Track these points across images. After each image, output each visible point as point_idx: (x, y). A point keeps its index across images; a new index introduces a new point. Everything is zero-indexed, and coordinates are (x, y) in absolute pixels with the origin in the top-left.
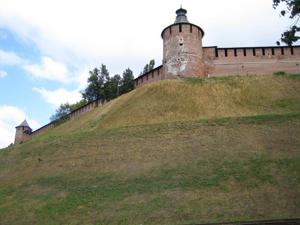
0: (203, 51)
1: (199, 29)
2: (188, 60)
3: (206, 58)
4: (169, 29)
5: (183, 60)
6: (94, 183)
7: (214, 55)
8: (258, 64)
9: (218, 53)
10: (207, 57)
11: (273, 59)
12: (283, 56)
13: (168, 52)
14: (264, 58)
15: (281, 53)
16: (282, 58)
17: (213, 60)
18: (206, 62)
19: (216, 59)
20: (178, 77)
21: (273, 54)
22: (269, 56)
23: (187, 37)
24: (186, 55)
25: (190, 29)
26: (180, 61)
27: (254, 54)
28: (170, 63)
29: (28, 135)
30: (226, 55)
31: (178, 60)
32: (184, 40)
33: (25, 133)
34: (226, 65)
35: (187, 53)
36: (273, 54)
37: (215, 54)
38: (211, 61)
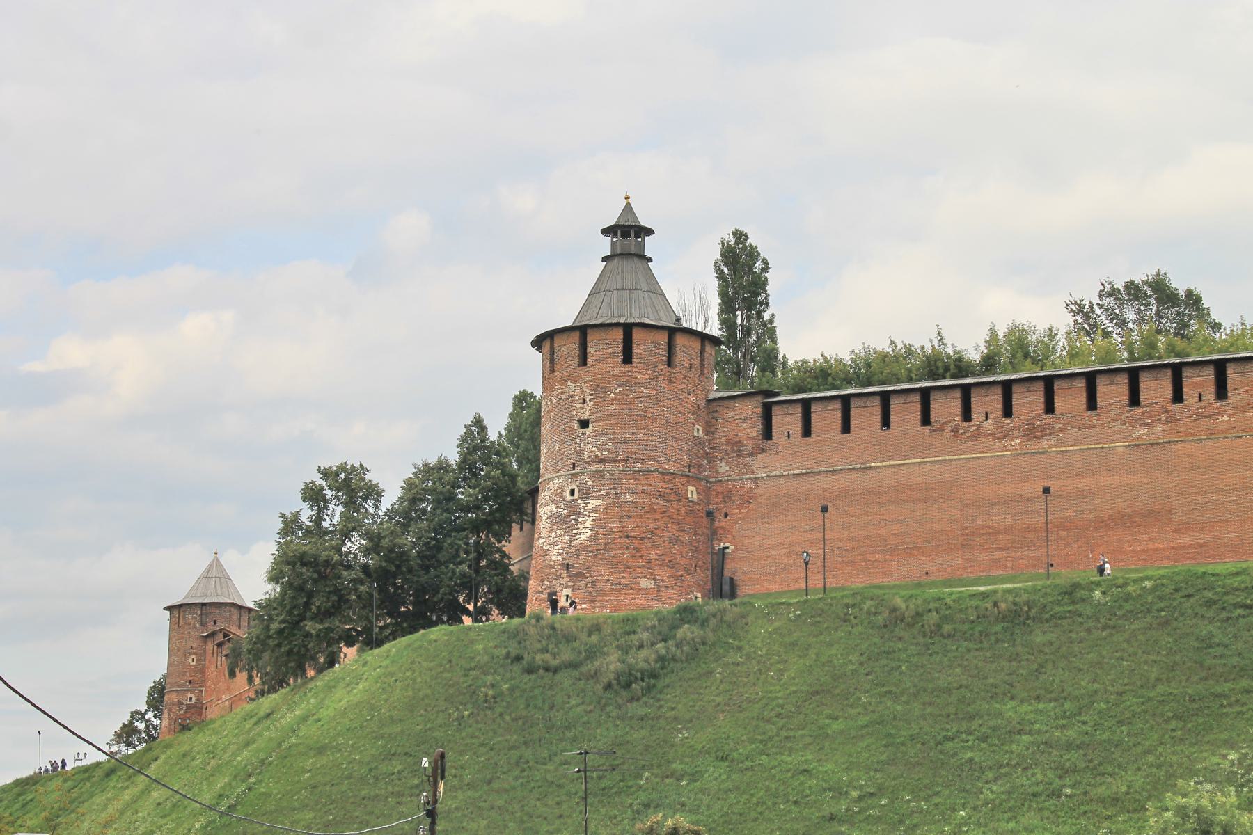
2: (608, 494)
5: (586, 496)
6: (1046, 654)
7: (756, 431)
10: (728, 442)
12: (1048, 419)
14: (964, 437)
16: (1046, 432)
17: (751, 454)
18: (723, 464)
19: (763, 450)
20: (564, 573)
22: (989, 425)
23: (605, 389)
24: (602, 471)
31: (568, 497)
32: (596, 404)
34: (801, 479)
35: (602, 460)
36: (1008, 412)
37: (760, 427)
38: (741, 460)
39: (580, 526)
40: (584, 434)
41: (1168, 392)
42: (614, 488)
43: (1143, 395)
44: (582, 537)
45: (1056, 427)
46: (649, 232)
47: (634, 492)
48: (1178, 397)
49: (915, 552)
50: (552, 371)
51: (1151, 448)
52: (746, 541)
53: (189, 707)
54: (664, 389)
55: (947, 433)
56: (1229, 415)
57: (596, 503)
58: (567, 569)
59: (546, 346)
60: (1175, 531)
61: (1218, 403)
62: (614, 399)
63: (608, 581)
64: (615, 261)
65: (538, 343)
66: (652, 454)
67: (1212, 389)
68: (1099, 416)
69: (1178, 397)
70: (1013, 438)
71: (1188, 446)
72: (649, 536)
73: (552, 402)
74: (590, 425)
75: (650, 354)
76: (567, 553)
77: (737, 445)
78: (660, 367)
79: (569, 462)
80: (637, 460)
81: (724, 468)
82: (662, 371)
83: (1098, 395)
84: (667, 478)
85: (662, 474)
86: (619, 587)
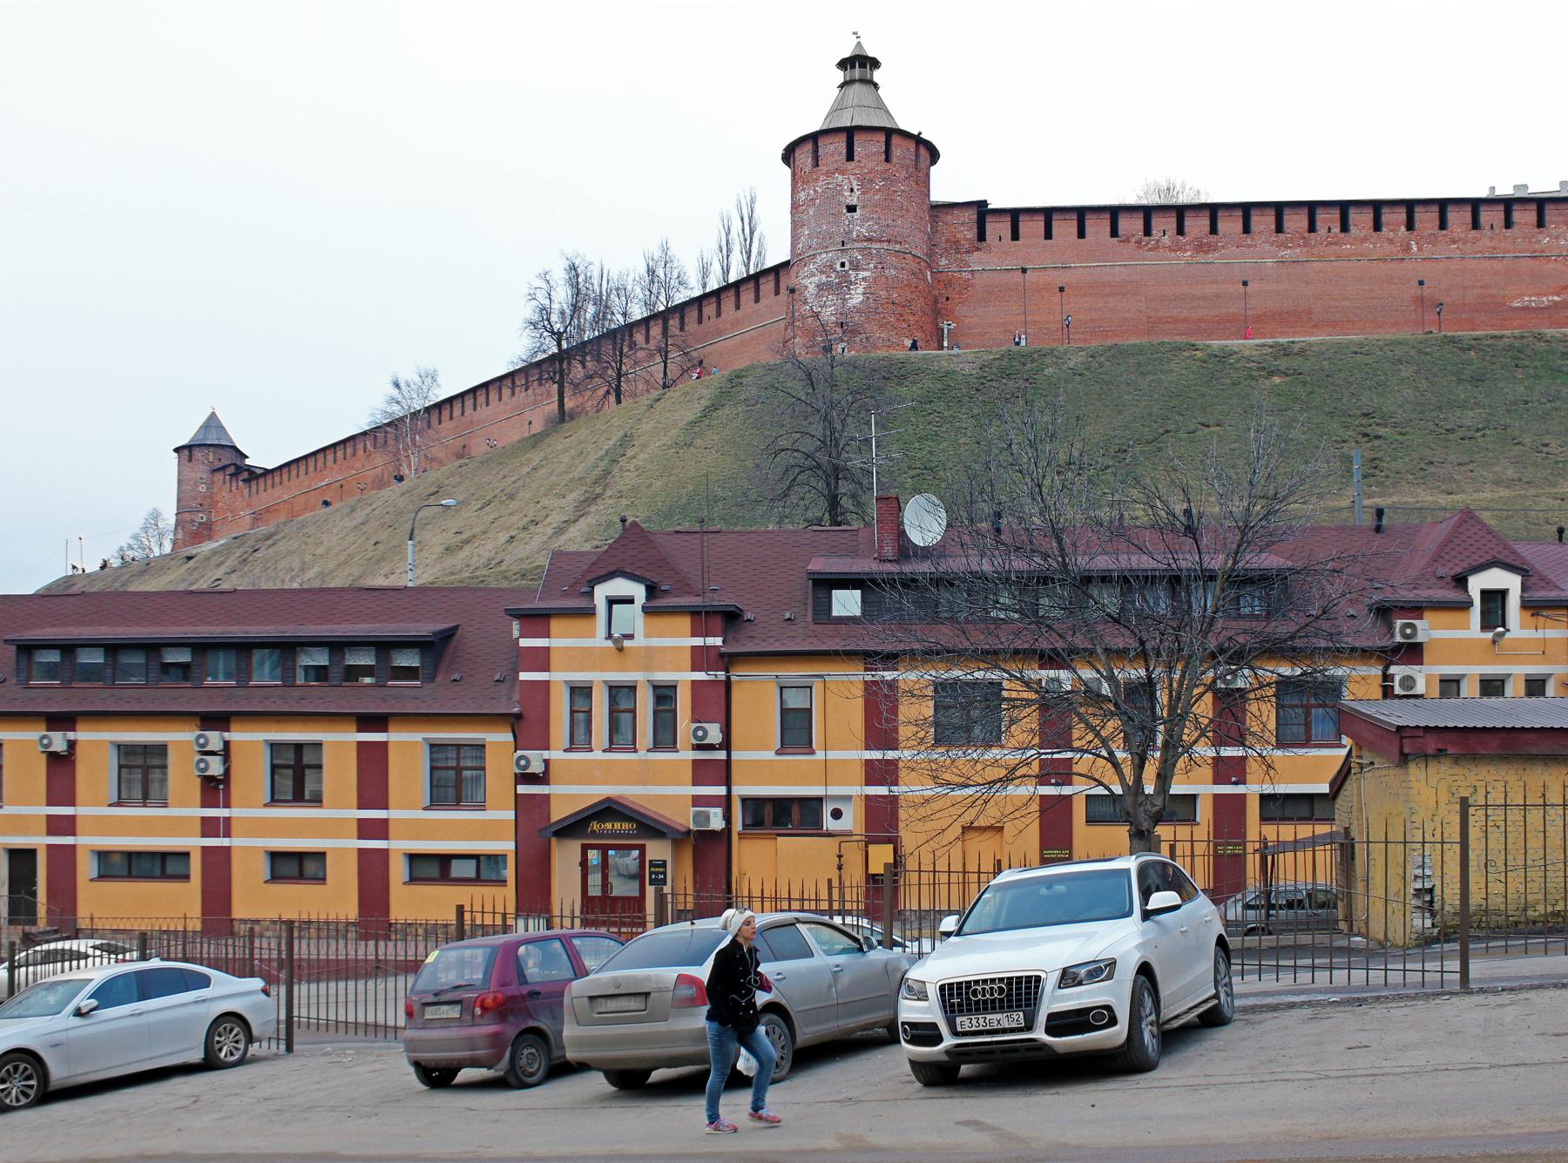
0: (934, 220)
1: (918, 140)
2: (875, 267)
3: (944, 245)
4: (809, 147)
5: (856, 267)
7: (971, 234)
8: (1124, 270)
9: (987, 228)
10: (947, 241)
11: (1180, 249)
12: (1213, 238)
13: (807, 233)
15: (1208, 229)
17: (968, 252)
19: (978, 249)
21: (1180, 230)
22: (1166, 240)
23: (871, 181)
25: (884, 148)
26: (846, 272)
27: (1114, 232)
28: (813, 275)
29: (241, 483)
30: (1015, 236)
31: (838, 268)
32: (863, 193)
33: (219, 477)
34: (1011, 274)
35: (869, 240)
36: (1180, 230)
37: (975, 230)
39: (853, 292)
40: (852, 217)
41: (1305, 224)
42: (881, 263)
43: (1286, 225)
44: (854, 301)
45: (1220, 244)
48: (1312, 228)
49: (1110, 334)
51: (1293, 265)
52: (966, 321)
53: (200, 524)
55: (1132, 245)
56: (1351, 244)
57: (866, 274)
58: (842, 327)
60: (1314, 326)
61: (1343, 234)
62: (879, 190)
63: (879, 338)
67: (1338, 225)
68: (1252, 238)
69: (1312, 228)
70: (1185, 251)
71: (1321, 264)
73: (815, 191)
74: (858, 210)
75: (904, 158)
76: (841, 314)
77: (955, 244)
79: (838, 240)
80: (896, 242)
81: (943, 262)
83: (1252, 223)
84: (917, 260)
86: (888, 343)
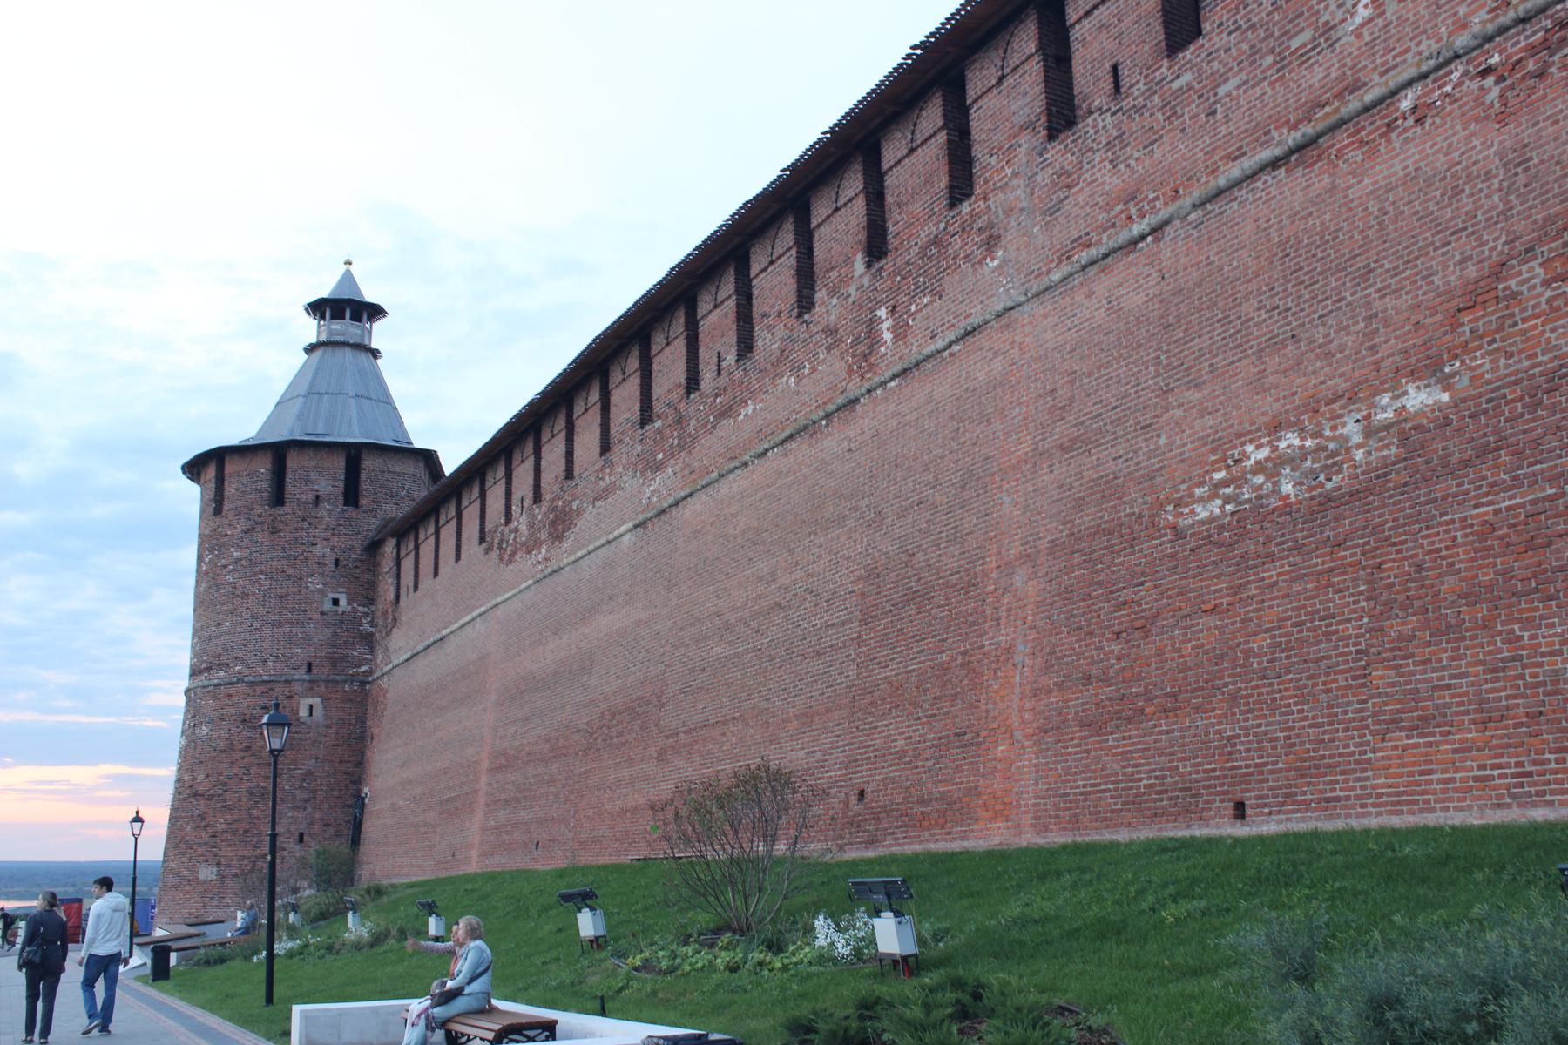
46: (376, 312)
47: (212, 721)
50: (218, 511)
54: (262, 544)
59: (211, 472)
64: (318, 353)
65: (194, 468)
66: (240, 654)
72: (220, 792)
78: (258, 510)
80: (220, 666)
82: (260, 516)
85: (252, 684)
